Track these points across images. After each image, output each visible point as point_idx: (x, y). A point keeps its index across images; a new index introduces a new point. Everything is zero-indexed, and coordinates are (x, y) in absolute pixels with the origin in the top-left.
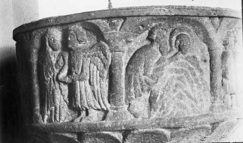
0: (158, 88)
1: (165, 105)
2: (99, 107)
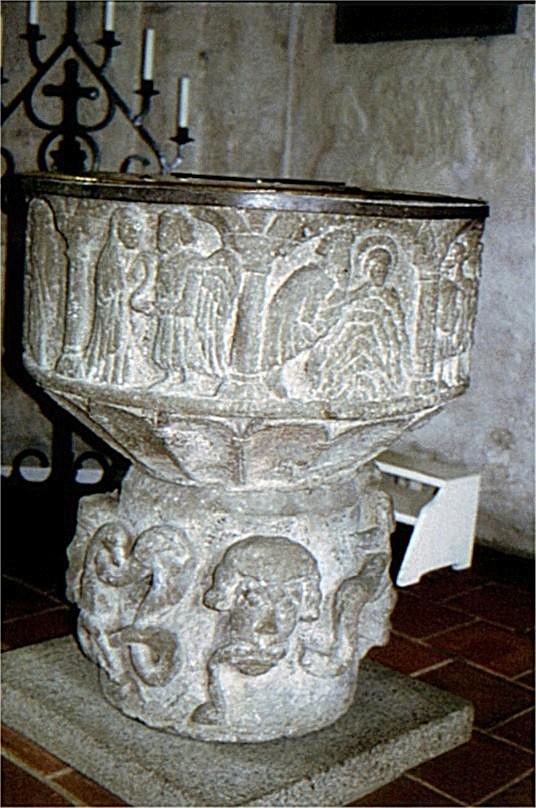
1: (335, 378)
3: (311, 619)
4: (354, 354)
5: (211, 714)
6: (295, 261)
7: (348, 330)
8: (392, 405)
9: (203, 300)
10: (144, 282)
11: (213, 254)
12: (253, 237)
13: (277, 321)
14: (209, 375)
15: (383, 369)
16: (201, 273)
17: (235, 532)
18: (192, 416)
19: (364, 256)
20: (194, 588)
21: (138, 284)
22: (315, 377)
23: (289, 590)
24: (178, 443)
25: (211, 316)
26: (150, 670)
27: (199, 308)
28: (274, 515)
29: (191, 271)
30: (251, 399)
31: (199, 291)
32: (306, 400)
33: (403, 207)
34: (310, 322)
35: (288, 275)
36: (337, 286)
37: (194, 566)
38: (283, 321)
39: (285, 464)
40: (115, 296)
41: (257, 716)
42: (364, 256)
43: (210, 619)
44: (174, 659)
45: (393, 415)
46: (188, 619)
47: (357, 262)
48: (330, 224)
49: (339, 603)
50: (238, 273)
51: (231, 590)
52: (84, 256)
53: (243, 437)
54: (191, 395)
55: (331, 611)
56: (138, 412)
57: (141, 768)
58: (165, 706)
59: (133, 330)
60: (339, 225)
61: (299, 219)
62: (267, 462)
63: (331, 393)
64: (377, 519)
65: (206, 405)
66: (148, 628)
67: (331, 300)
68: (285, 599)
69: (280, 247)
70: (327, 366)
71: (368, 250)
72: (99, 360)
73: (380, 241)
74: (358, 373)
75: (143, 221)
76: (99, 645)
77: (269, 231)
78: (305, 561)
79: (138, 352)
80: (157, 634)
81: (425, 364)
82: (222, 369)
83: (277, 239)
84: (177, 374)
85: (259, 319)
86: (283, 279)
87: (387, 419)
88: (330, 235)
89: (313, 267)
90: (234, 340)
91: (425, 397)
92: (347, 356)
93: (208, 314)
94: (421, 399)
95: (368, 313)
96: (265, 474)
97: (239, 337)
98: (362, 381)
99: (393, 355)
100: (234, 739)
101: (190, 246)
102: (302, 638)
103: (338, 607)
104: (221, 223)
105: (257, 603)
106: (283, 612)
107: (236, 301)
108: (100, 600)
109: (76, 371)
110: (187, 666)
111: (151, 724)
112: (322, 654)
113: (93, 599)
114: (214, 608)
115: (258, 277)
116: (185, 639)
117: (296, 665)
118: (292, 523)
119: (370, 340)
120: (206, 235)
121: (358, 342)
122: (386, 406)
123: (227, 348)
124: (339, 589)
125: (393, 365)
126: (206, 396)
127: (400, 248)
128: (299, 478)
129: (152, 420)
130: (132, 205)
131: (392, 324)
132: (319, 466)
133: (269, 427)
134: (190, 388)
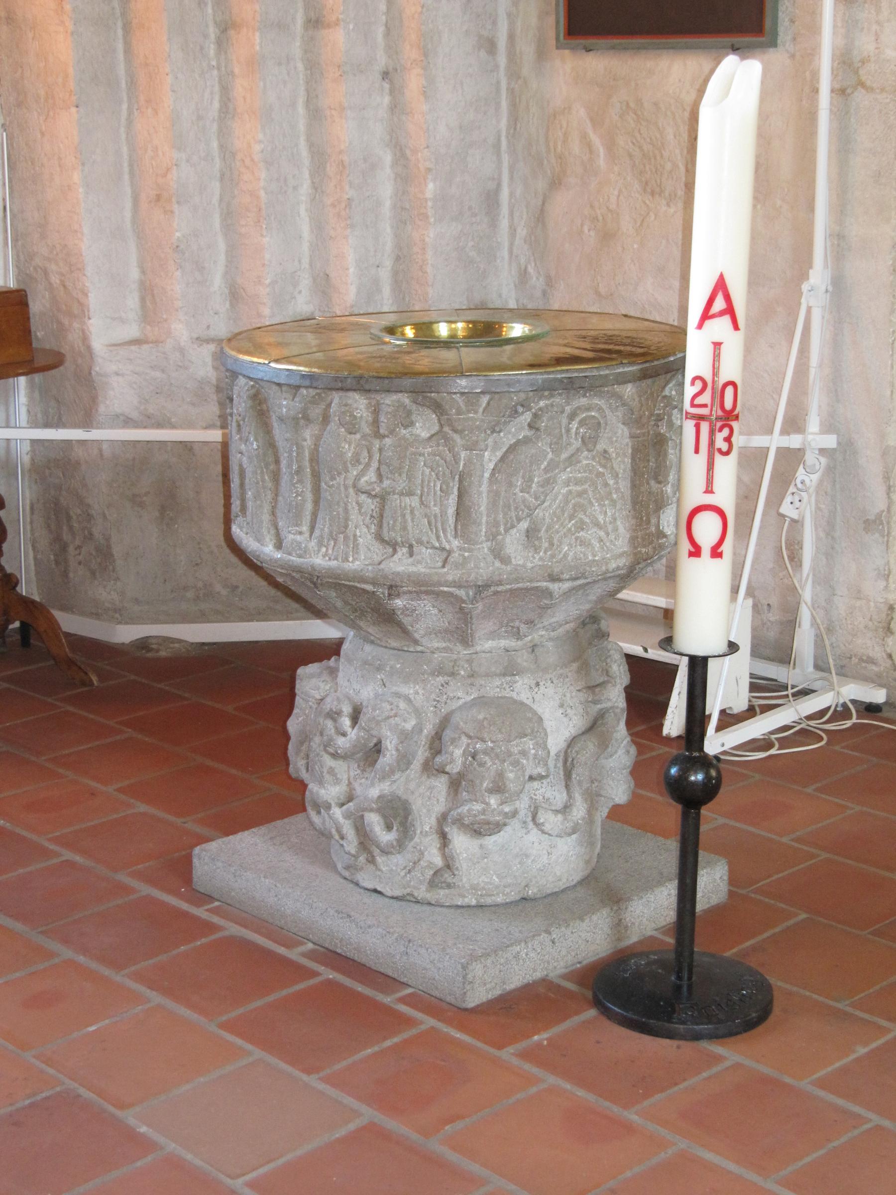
0: (543, 514)
1: (555, 541)
2: (437, 545)
3: (541, 777)
4: (571, 517)
5: (447, 877)
6: (510, 436)
7: (563, 496)
8: (613, 561)
9: (426, 479)
10: (368, 465)
11: (432, 436)
12: (468, 418)
13: (497, 494)
14: (436, 548)
15: (601, 528)
16: (422, 455)
17: (460, 694)
18: (423, 588)
19: (574, 425)
20: (421, 754)
21: (361, 467)
22: (536, 543)
23: (515, 750)
24: (408, 612)
25: (435, 494)
26: (385, 837)
27: (422, 487)
28: (496, 675)
29: (414, 454)
30: (479, 568)
31: (422, 470)
32: (530, 565)
33: (606, 376)
34: (528, 493)
35: (504, 449)
36: (550, 456)
37: (421, 731)
38: (503, 494)
39: (512, 624)
40: (340, 480)
41: (494, 877)
42: (574, 425)
43: (441, 784)
44: (408, 824)
45: (613, 571)
46: (418, 786)
47: (568, 431)
48: (541, 398)
49: (570, 760)
50: (458, 453)
51: (458, 752)
52: (306, 440)
53: (472, 604)
54: (421, 569)
55: (562, 768)
56: (369, 587)
57: (384, 932)
58: (403, 874)
59: (360, 510)
60: (549, 399)
61: (512, 399)
62: (495, 624)
63: (553, 556)
64: (607, 672)
65: (436, 578)
66: (379, 797)
67: (546, 470)
68: (511, 759)
69: (495, 426)
70: (547, 531)
71: (578, 419)
72: (329, 540)
73: (588, 409)
74: (577, 534)
75: (362, 407)
76: (330, 817)
77: (483, 412)
78: (530, 720)
79: (365, 530)
80: (391, 801)
81: (641, 518)
82: (449, 542)
83: (491, 418)
84: (405, 550)
85: (480, 493)
86: (499, 454)
87: (609, 575)
88: (541, 409)
89: (526, 441)
90: (457, 514)
91: (644, 550)
92: (565, 520)
93: (432, 493)
94: (640, 552)
95: (582, 477)
96: (492, 635)
97: (463, 511)
98: (581, 541)
99: (609, 514)
100: (474, 902)
101: (410, 429)
102: (534, 797)
103: (568, 764)
104: (438, 408)
105: (485, 763)
106: (512, 771)
107: (457, 477)
108: (328, 772)
109: (305, 552)
110: (421, 832)
111: (389, 893)
112: (557, 812)
113: (322, 773)
114: (444, 772)
115: (477, 454)
116: (417, 804)
117: (531, 825)
118: (515, 682)
119: (585, 502)
120: (424, 417)
121: (574, 506)
122: (607, 564)
123: (451, 521)
124: (569, 746)
125: (611, 523)
126: (434, 568)
127: (607, 412)
128: (525, 636)
129: (383, 593)
130: (351, 394)
131: (606, 485)
132: (546, 623)
133: (496, 593)
134: (419, 562)
